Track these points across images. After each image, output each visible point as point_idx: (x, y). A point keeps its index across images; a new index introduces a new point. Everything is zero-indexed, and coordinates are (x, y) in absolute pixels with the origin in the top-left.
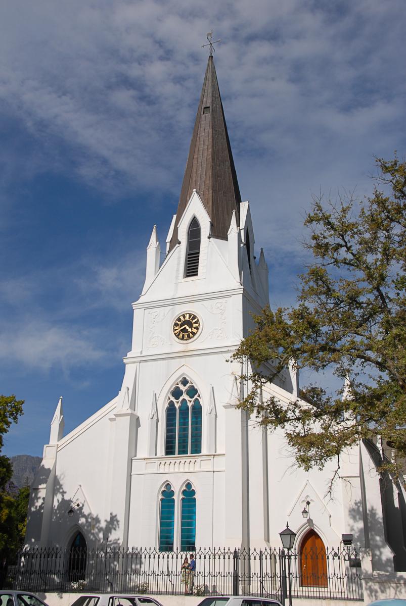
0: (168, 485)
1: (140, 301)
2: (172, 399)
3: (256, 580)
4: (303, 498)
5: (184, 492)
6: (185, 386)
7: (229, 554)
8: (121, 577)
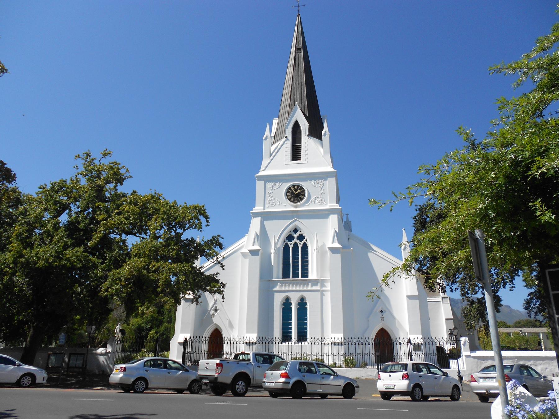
3: (406, 357)
6: (296, 233)
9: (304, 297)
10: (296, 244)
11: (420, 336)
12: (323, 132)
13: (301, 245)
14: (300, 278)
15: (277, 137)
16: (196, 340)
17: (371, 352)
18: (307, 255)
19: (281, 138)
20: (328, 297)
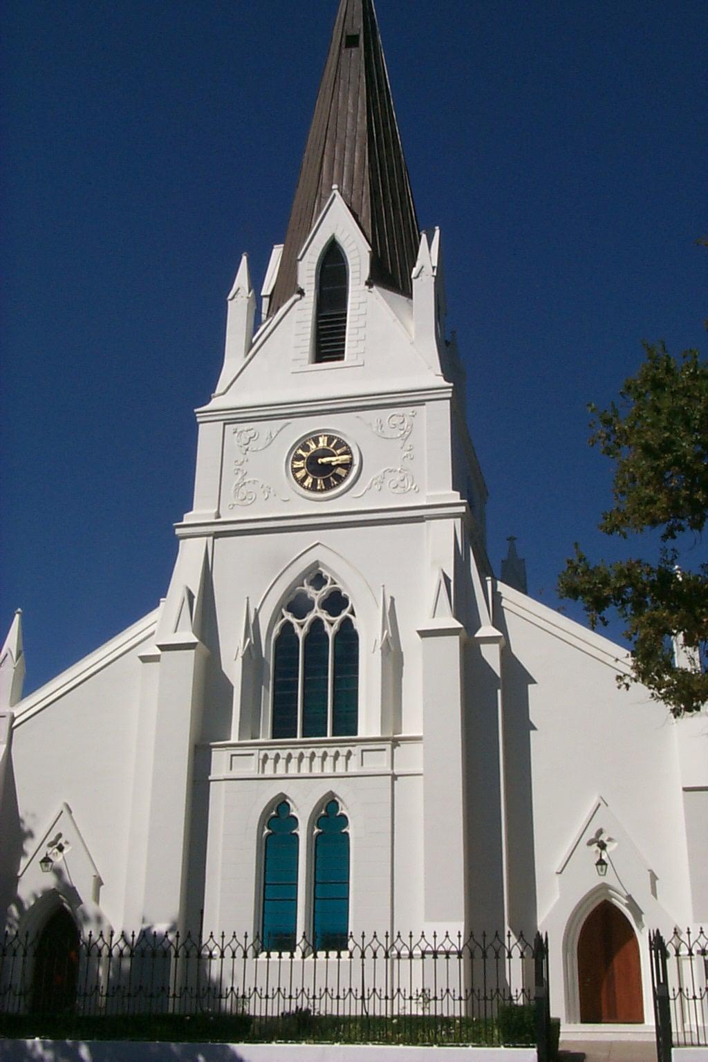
1: (213, 405)
2: (289, 616)
4: (591, 834)
6: (318, 589)
10: (317, 623)
12: (415, 271)
13: (336, 627)
14: (329, 737)
20: (413, 795)
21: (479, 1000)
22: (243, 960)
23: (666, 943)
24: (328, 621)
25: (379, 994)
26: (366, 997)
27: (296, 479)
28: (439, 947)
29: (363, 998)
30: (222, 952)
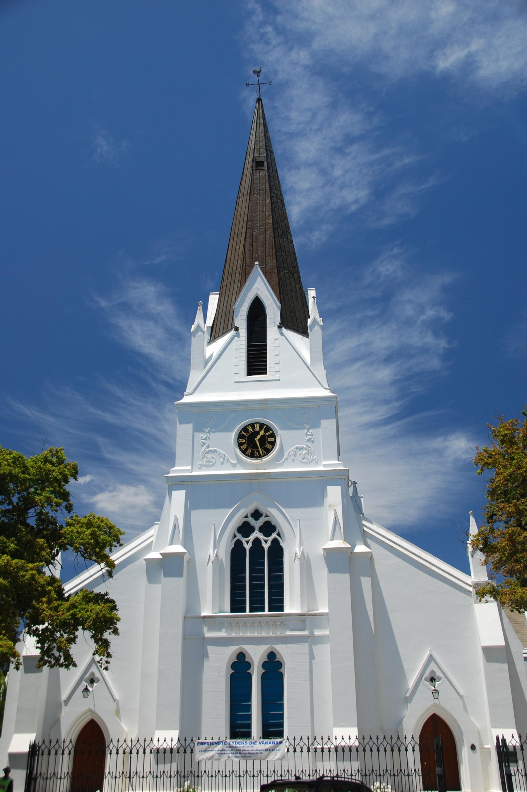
0: (241, 656)
2: (239, 536)
4: (427, 674)
5: (265, 665)
7: (302, 746)
8: (210, 782)
9: (244, 652)
10: (257, 541)
11: (353, 732)
12: (309, 321)
13: (269, 544)
15: (218, 328)
16: (301, 744)
17: (412, 767)
18: (281, 563)
19: (225, 331)
21: (222, 777)
22: (315, 753)
23: (106, 746)
24: (263, 539)
25: (57, 776)
26: (132, 776)
27: (241, 450)
28: (509, 743)
29: (130, 777)
30: (131, 751)
